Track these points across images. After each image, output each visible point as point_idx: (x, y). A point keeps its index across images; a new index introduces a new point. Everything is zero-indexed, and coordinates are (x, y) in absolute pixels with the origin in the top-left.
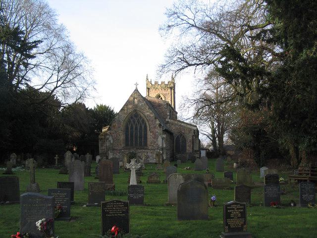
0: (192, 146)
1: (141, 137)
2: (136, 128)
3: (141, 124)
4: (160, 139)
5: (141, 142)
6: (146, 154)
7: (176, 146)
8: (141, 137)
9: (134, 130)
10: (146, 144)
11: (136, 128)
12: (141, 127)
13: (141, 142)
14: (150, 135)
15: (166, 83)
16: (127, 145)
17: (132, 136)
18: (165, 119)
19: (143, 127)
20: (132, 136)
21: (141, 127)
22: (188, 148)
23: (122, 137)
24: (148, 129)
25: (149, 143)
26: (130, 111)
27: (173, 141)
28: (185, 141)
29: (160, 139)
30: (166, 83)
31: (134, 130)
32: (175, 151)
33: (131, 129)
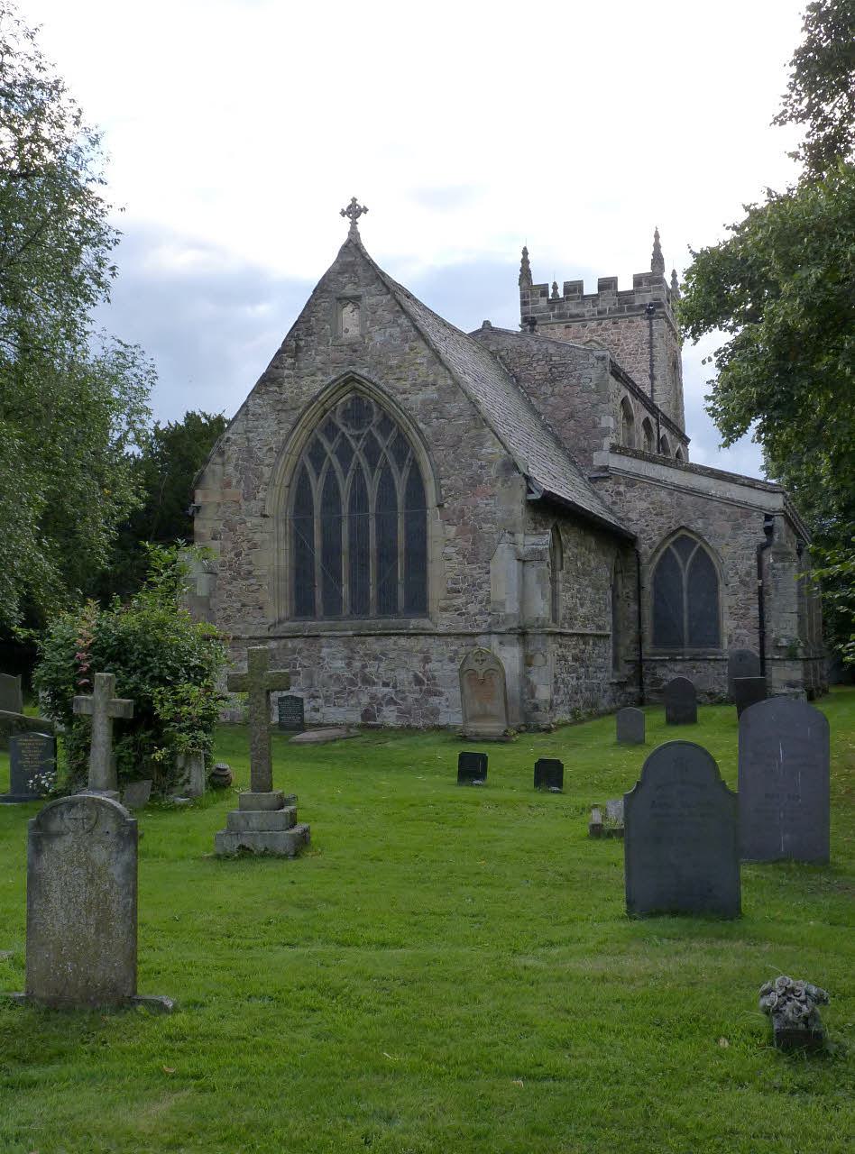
0: (754, 612)
1: (387, 555)
2: (359, 500)
3: (359, 471)
4: (504, 566)
5: (387, 591)
6: (416, 665)
7: (656, 615)
8: (387, 555)
9: (345, 509)
10: (418, 604)
11: (359, 500)
12: (387, 484)
13: (387, 591)
14: (441, 536)
15: (625, 285)
16: (303, 606)
17: (331, 552)
18: (586, 453)
19: (372, 491)
20: (331, 552)
21: (387, 484)
22: (728, 625)
23: (273, 558)
24: (431, 500)
25: (436, 591)
26: (317, 388)
27: (640, 588)
28: (705, 567)
29: (504, 566)
30: (625, 285)
31: (345, 509)
32: (648, 648)
33: (325, 504)
